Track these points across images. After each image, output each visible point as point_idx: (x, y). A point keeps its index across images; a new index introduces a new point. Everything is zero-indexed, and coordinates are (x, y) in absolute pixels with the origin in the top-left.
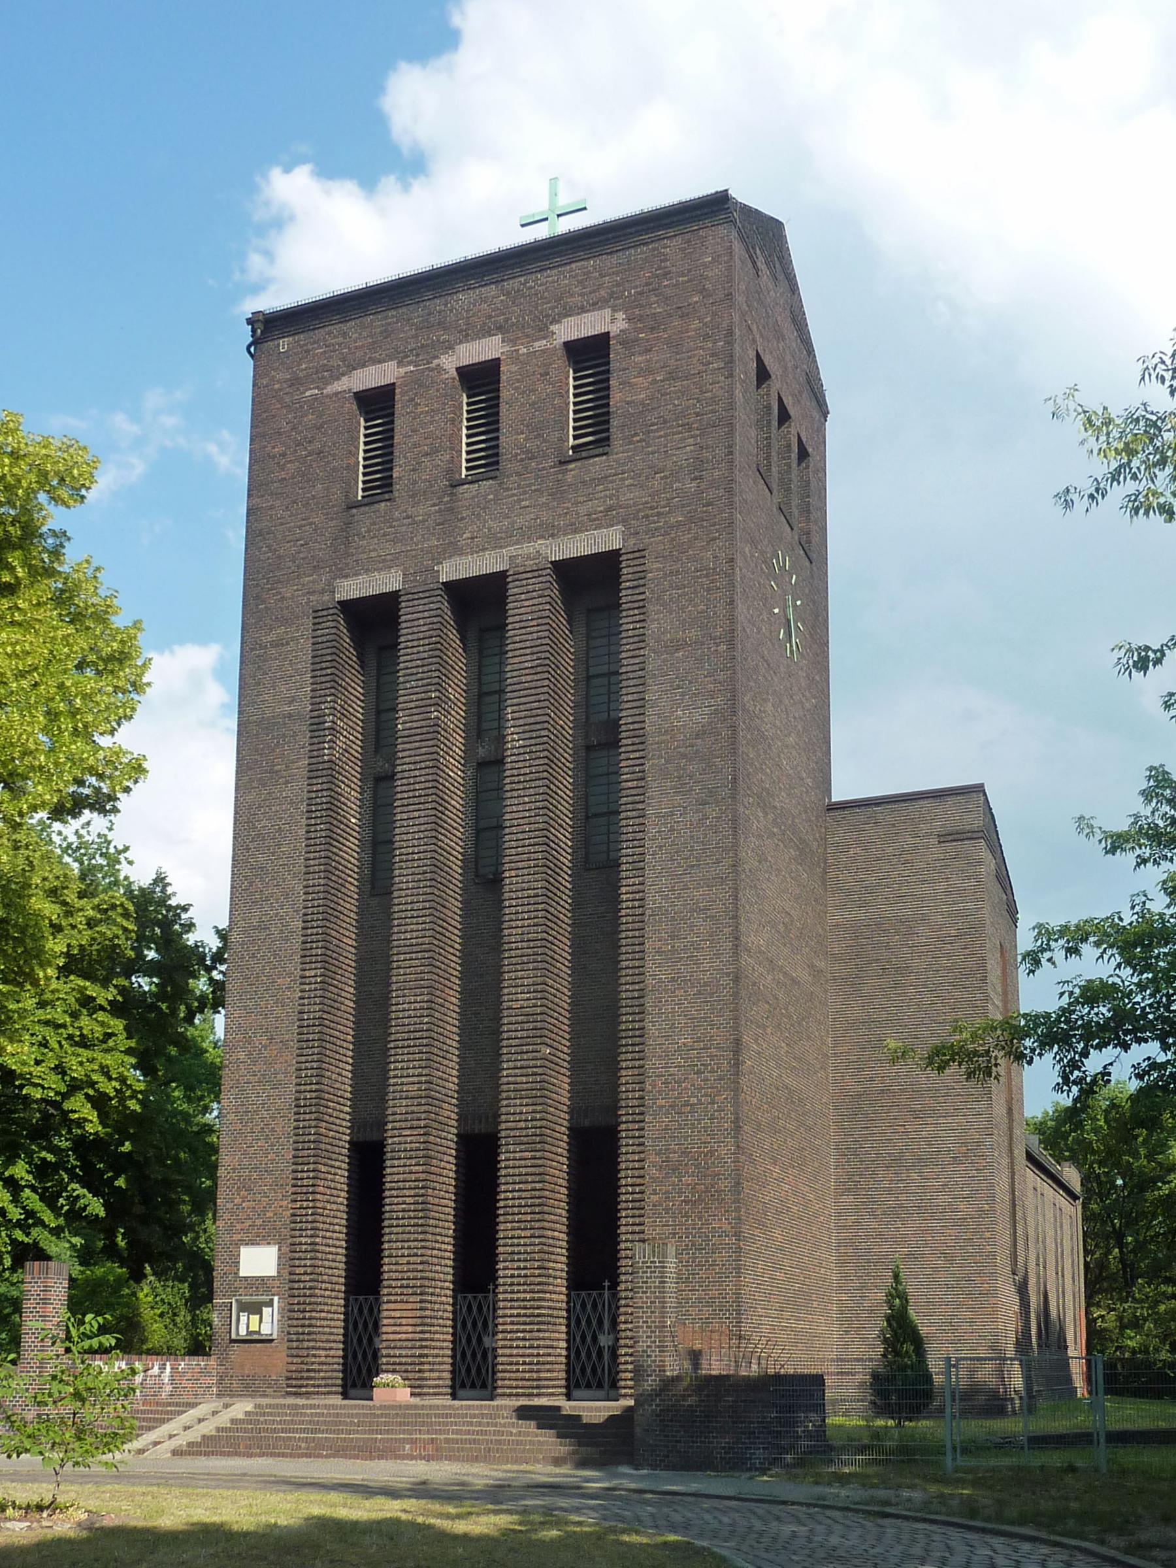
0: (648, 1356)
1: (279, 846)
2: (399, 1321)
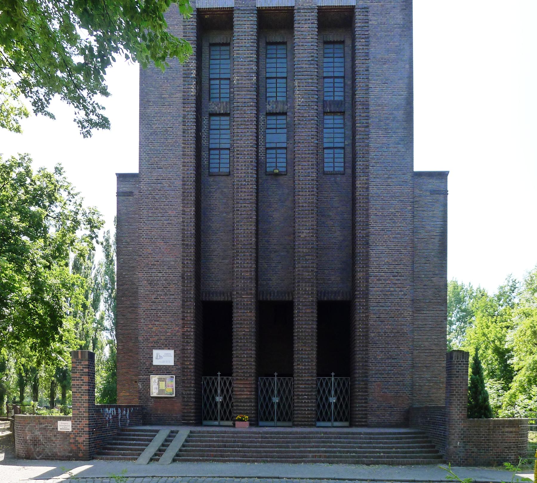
0: (459, 410)
1: (166, 139)
2: (242, 389)
